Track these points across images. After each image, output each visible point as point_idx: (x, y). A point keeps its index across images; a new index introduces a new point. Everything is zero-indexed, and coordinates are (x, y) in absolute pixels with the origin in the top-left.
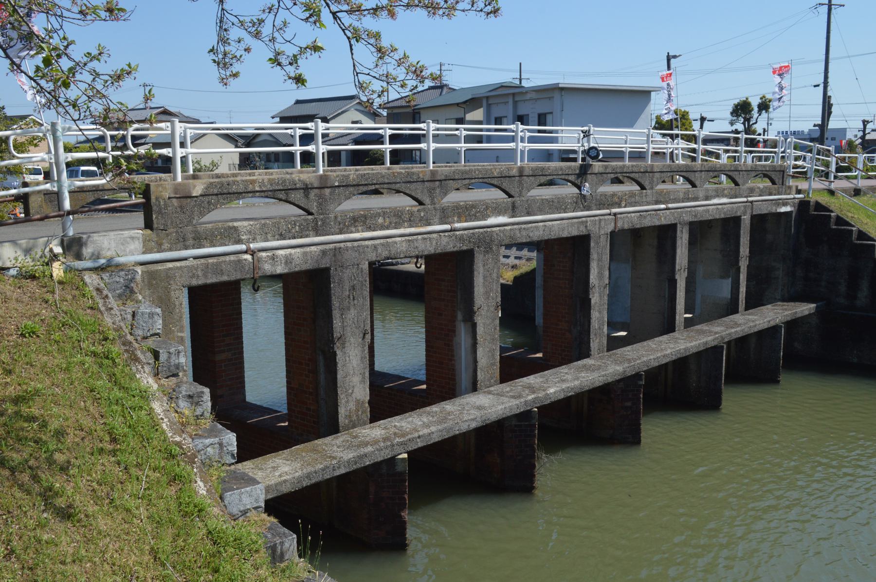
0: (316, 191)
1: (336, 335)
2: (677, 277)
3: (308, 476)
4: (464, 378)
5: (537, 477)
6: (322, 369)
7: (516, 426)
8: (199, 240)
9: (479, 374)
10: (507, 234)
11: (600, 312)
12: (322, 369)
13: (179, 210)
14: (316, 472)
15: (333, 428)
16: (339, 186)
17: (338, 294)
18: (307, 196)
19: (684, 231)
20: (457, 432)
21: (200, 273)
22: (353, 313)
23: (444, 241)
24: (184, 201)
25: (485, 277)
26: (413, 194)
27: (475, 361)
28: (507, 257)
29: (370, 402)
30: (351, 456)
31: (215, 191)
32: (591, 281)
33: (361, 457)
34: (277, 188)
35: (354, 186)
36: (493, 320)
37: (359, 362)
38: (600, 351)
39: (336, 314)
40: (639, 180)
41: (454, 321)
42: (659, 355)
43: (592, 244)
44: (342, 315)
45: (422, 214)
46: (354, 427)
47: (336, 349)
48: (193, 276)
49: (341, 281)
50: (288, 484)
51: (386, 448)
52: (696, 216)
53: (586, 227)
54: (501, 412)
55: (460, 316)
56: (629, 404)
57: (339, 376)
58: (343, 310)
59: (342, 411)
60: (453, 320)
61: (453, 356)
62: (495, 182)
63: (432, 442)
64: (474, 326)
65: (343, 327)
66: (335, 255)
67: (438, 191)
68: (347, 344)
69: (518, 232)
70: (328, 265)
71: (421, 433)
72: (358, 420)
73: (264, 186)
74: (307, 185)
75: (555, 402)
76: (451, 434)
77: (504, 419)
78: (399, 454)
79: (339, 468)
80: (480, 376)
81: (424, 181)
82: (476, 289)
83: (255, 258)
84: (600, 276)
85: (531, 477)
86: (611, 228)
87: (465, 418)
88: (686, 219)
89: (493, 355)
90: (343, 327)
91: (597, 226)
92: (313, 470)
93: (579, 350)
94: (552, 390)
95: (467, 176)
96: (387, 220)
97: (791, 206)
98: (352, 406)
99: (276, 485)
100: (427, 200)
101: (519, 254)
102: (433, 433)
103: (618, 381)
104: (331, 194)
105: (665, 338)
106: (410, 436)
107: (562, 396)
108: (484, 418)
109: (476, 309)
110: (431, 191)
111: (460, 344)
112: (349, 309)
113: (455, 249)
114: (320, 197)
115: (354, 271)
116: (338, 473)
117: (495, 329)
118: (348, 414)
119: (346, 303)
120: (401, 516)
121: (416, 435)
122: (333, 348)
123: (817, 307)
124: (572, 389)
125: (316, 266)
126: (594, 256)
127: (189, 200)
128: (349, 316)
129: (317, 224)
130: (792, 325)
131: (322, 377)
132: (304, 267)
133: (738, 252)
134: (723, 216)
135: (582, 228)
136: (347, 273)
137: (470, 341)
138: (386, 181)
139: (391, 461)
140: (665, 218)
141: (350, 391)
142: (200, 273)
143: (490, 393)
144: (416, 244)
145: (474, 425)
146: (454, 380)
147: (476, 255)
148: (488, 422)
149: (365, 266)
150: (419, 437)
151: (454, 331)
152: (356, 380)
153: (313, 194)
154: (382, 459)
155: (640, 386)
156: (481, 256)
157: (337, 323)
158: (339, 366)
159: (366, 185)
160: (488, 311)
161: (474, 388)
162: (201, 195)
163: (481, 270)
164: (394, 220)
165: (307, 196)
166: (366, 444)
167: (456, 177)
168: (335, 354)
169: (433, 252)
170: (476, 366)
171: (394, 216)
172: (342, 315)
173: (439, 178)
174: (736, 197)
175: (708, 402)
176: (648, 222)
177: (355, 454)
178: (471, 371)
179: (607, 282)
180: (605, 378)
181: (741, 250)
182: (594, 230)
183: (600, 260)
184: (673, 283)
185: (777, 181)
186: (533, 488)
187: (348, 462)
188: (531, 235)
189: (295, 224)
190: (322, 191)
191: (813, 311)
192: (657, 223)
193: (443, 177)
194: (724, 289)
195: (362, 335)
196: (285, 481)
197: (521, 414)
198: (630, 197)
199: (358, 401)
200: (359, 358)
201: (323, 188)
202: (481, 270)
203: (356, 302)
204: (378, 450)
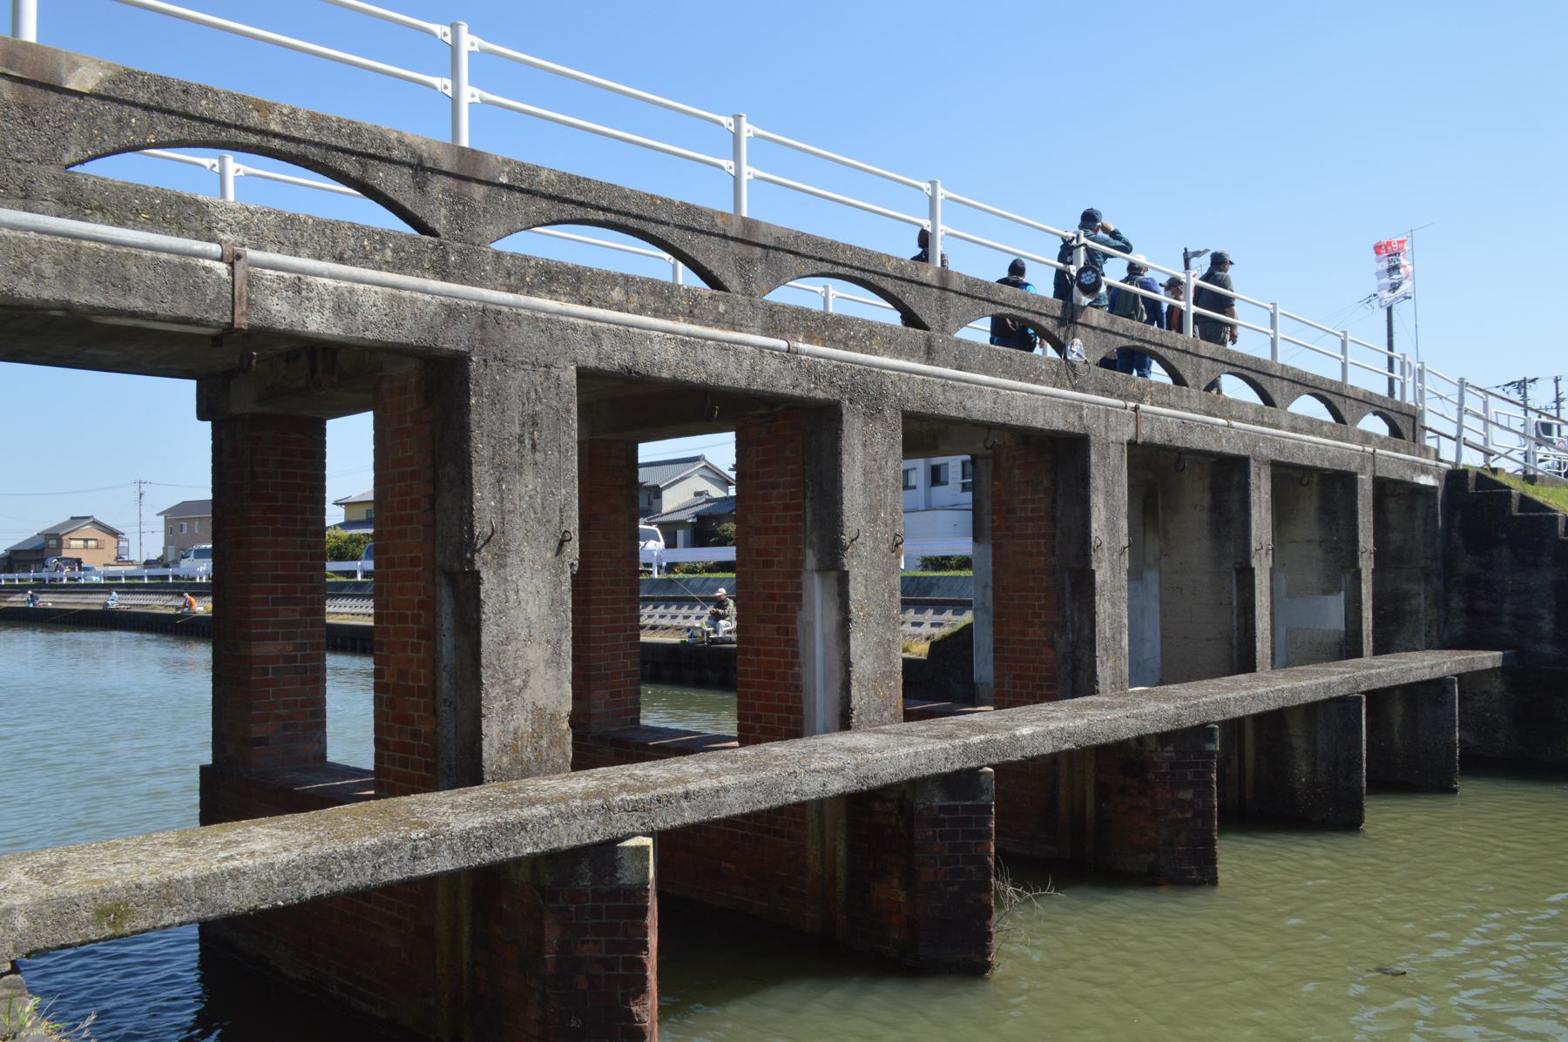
0: (449, 181)
1: (481, 529)
2: (1254, 563)
3: (323, 866)
4: (821, 701)
5: (996, 942)
6: (446, 622)
7: (942, 809)
8: (76, 202)
9: (854, 691)
10: (917, 389)
11: (1113, 604)
12: (446, 622)
13: (18, 113)
14: (350, 857)
15: (469, 772)
16: (509, 187)
17: (490, 427)
18: (421, 187)
19: (1263, 475)
20: (794, 798)
21: (47, 268)
22: (527, 485)
23: (771, 365)
24: (38, 97)
25: (866, 472)
26: (700, 259)
27: (847, 663)
28: (918, 624)
29: (574, 721)
30: (476, 822)
31: (143, 97)
32: (1094, 535)
33: (507, 829)
34: (333, 141)
35: (550, 197)
36: (888, 573)
37: (545, 610)
38: (1117, 685)
39: (482, 475)
40: (1175, 363)
41: (799, 574)
42: (1244, 693)
43: (1094, 458)
44: (499, 481)
45: (722, 308)
46: (526, 773)
47: (478, 565)
48: (23, 270)
49: (497, 395)
50: (247, 884)
51: (589, 812)
52: (1281, 451)
53: (1081, 417)
54: (905, 763)
55: (811, 560)
56: (1187, 795)
57: (485, 638)
58: (502, 472)
59: (493, 732)
60: (795, 571)
61: (796, 655)
62: (888, 284)
63: (724, 813)
64: (843, 579)
65: (502, 514)
66: (482, 326)
67: (759, 268)
68: (512, 559)
69: (939, 391)
70: (462, 347)
71: (692, 787)
72: (541, 761)
73: (298, 126)
74: (420, 157)
75: (1033, 759)
76: (776, 801)
77: (912, 782)
78: (633, 835)
79: (433, 852)
80: (858, 697)
81: (725, 237)
82: (846, 495)
83: (240, 273)
84: (1112, 529)
85: (982, 938)
86: (1128, 433)
87: (815, 765)
88: (1264, 452)
89: (888, 654)
90: (502, 514)
91: (1102, 422)
92: (341, 848)
93: (1073, 677)
94: (1026, 731)
95: (826, 256)
96: (635, 298)
97: (1437, 477)
98: (521, 720)
99: (200, 882)
100: (733, 283)
101: (938, 618)
102: (726, 790)
103: (1163, 738)
104: (487, 198)
105: (1242, 677)
106: (660, 791)
107: (1048, 749)
108: (863, 771)
109: (846, 539)
110: (743, 265)
111: (812, 625)
112: (519, 470)
113: (798, 392)
114: (458, 198)
115: (538, 378)
116: (426, 868)
117: (892, 595)
118: (509, 740)
119: (512, 453)
120: (630, 1016)
121: (680, 790)
122: (471, 562)
123: (1505, 658)
124: (1071, 735)
125: (427, 340)
126: (1098, 482)
127: (54, 97)
128: (519, 488)
129: (445, 258)
130: (1468, 679)
131: (447, 644)
132: (393, 335)
133: (1356, 541)
134: (1326, 465)
135: (1072, 418)
136: (517, 381)
137: (833, 617)
138: (634, 210)
139: (605, 853)
140: (1228, 441)
141: (518, 682)
142: (47, 268)
143: (882, 732)
144: (701, 356)
145: (837, 786)
146: (799, 711)
147: (847, 417)
148: (874, 783)
149: (570, 375)
150: (687, 796)
151: (799, 598)
152: (536, 655)
153: (437, 185)
154: (574, 842)
155: (1211, 754)
156: (858, 423)
157: (484, 499)
158: (488, 610)
159: (581, 204)
160: (875, 550)
161: (844, 722)
162: (93, 95)
163: (859, 453)
164: (651, 302)
165: (421, 187)
166: (532, 803)
167: (802, 250)
168: (476, 578)
169: (743, 384)
170: (848, 674)
171: (653, 293)
172: (499, 481)
173: (762, 241)
174: (1342, 440)
175: (1335, 815)
176: (1197, 441)
177: (489, 819)
178: (836, 687)
179: (1125, 542)
180: (1139, 723)
181: (1361, 537)
182: (1096, 429)
183: (1109, 494)
184: (1245, 575)
185: (1405, 432)
186: (987, 966)
187: (466, 837)
188: (969, 404)
189: (382, 243)
190: (465, 185)
191: (1498, 664)
192: (1215, 448)
193: (770, 241)
194: (1331, 614)
195: (554, 544)
196: (235, 874)
197: (957, 774)
198: (1159, 391)
199: (538, 713)
200: (545, 601)
201: (469, 179)
202: (859, 453)
203: (539, 456)
204: (561, 815)
